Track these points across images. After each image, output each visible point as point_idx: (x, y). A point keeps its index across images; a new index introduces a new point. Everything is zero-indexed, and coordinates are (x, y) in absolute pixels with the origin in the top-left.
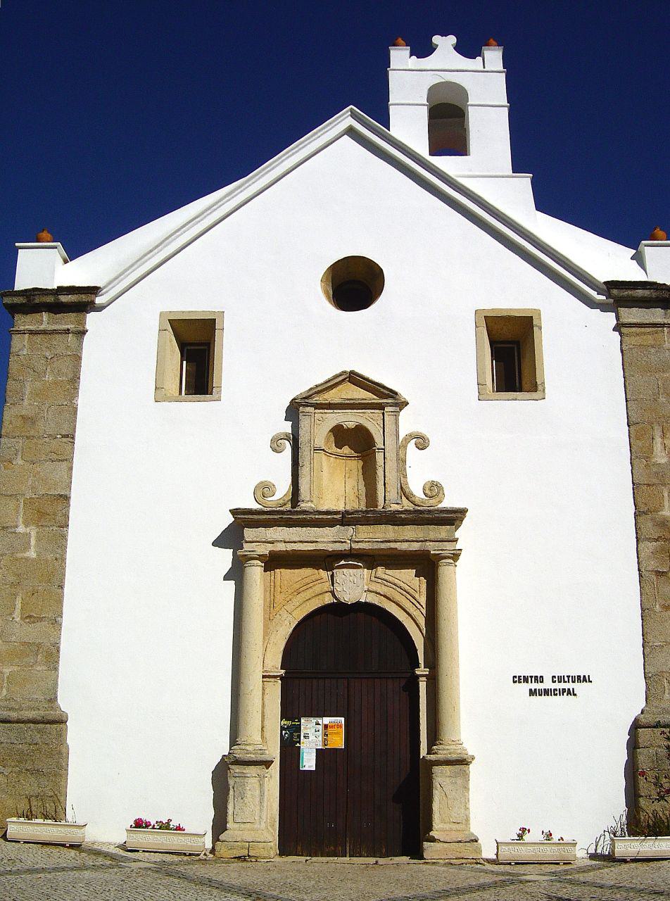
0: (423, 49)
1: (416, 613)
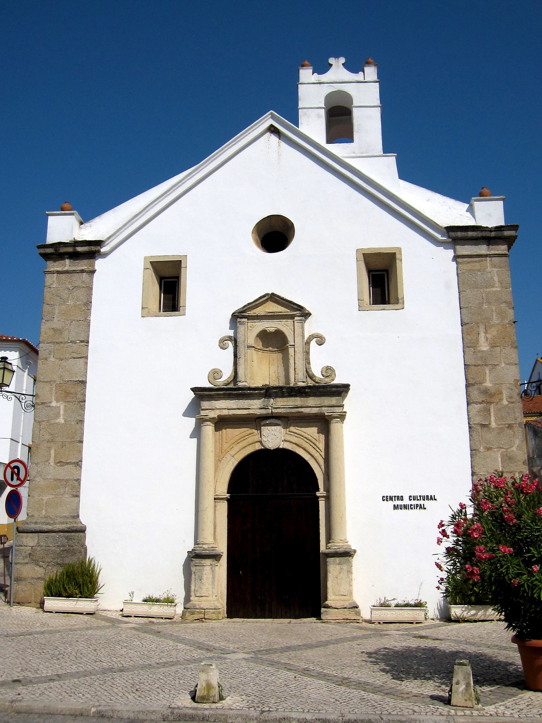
0: (322, 68)
1: (316, 455)
